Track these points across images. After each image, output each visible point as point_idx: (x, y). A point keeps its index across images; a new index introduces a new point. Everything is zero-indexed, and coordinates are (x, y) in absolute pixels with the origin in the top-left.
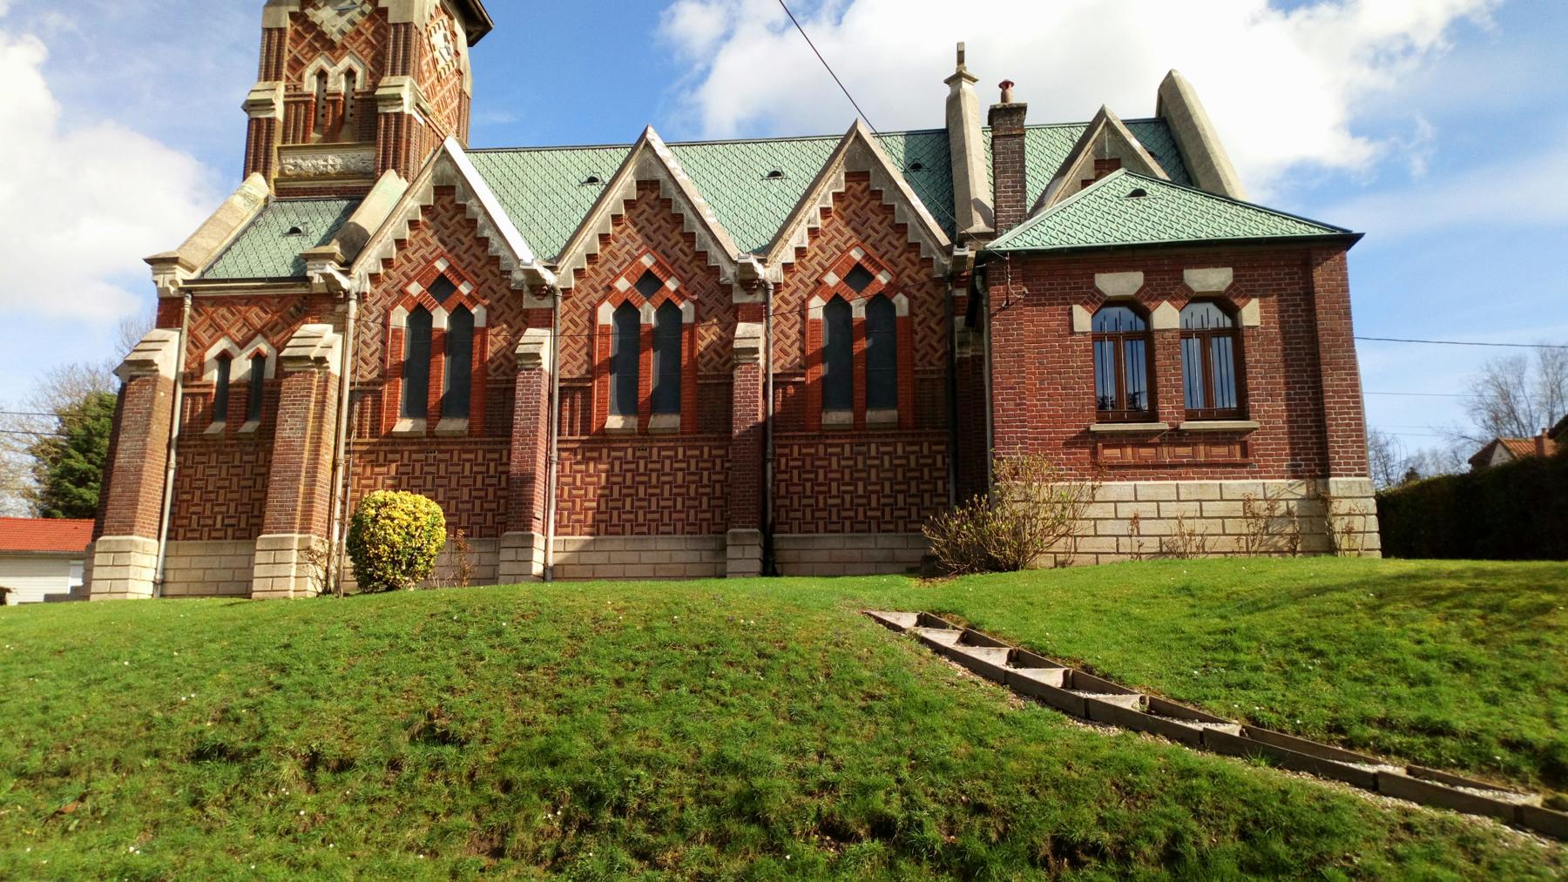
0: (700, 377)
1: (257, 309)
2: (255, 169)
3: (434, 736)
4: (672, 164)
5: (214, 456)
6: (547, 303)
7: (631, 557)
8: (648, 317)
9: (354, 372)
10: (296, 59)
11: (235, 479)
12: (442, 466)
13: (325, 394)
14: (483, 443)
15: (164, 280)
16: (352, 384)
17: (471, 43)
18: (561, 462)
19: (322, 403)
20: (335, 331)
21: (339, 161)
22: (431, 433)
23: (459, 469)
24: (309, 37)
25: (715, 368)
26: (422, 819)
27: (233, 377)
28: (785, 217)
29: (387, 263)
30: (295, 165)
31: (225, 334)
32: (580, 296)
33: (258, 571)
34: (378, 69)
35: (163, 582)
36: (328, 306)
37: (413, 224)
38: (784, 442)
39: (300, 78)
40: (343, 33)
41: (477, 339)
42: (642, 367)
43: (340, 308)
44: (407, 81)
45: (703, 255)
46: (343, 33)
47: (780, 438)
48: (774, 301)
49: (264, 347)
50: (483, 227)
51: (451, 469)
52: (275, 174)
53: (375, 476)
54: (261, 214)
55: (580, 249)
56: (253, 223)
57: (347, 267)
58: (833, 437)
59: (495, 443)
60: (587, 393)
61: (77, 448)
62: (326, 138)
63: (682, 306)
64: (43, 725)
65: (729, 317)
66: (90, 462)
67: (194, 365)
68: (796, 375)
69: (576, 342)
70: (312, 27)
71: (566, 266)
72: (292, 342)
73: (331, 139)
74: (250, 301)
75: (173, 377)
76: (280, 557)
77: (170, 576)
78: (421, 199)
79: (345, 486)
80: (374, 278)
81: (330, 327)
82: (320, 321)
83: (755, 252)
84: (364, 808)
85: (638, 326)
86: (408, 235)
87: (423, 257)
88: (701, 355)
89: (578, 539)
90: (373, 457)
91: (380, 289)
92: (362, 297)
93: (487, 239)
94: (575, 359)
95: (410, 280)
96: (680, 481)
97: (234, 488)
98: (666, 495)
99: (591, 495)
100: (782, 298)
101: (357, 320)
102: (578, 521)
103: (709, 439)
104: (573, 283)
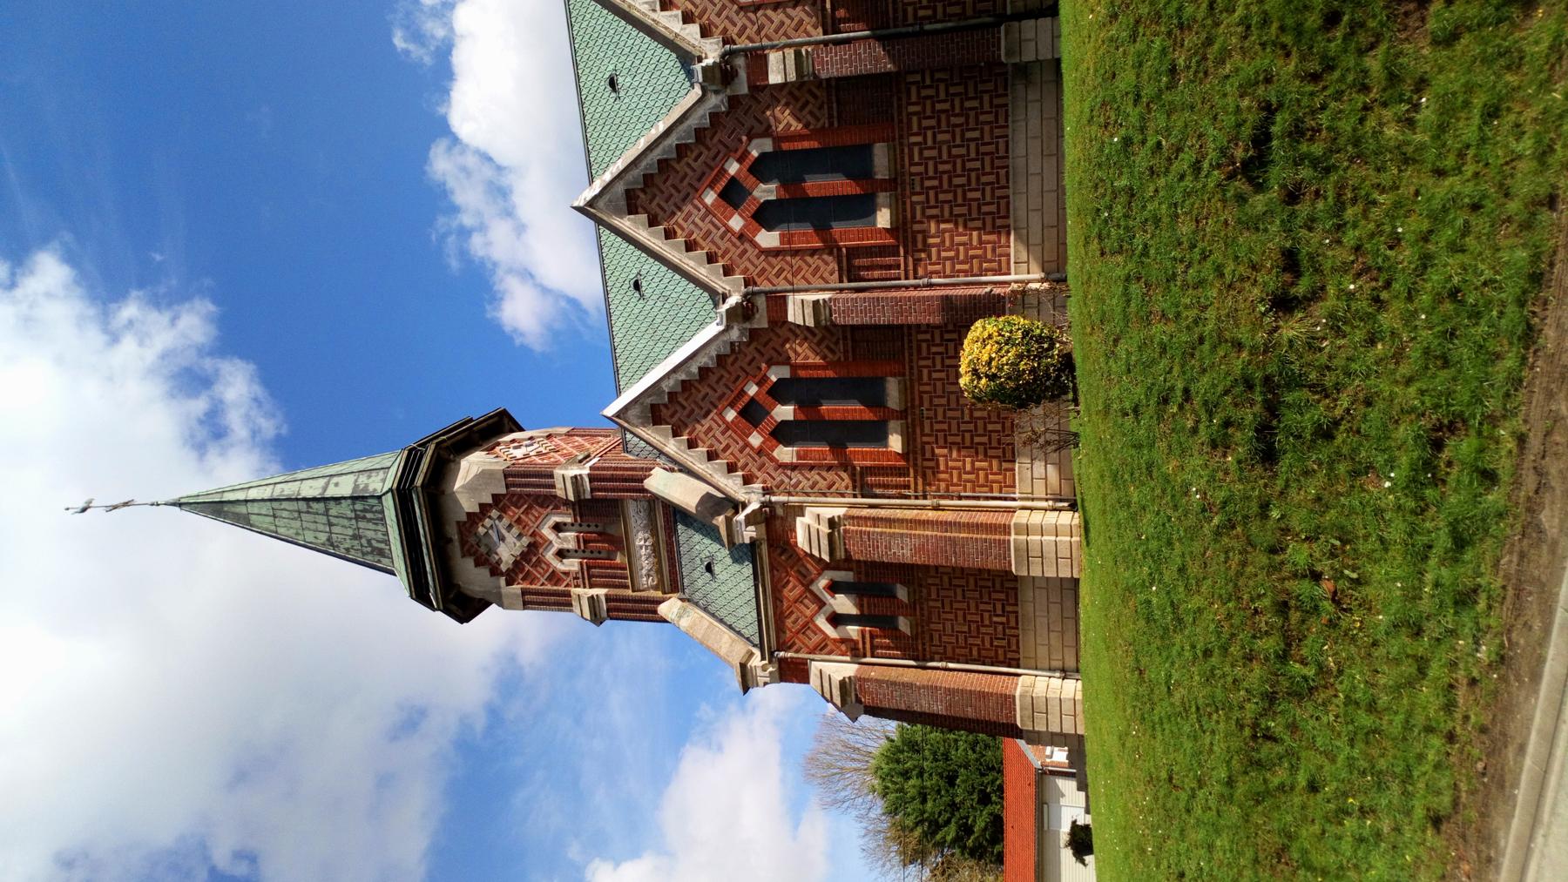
0: (831, 124)
1: (785, 591)
2: (655, 612)
3: (1253, 169)
4: (608, 177)
5: (933, 626)
6: (761, 302)
7: (1035, 184)
8: (769, 191)
9: (843, 495)
10: (549, 579)
11: (956, 605)
12: (936, 401)
13: (866, 519)
14: (911, 361)
15: (762, 677)
16: (855, 496)
17: (521, 429)
18: (930, 274)
19: (876, 521)
20: (803, 515)
21: (641, 535)
22: (902, 415)
23: (939, 384)
24: (527, 567)
25: (821, 108)
26: (1371, 123)
27: (854, 611)
28: (677, 277)
29: (731, 468)
30: (648, 576)
31: (811, 620)
32: (751, 268)
33: (1051, 573)
34: (550, 501)
35: (1063, 670)
36: (778, 522)
37: (692, 444)
38: (900, 14)
39: (567, 574)
40: (520, 536)
41: (802, 373)
42: (823, 193)
43: (780, 512)
44: (558, 472)
45: (699, 133)
46: (520, 536)
47: (895, 19)
48: (743, 43)
49: (823, 582)
50: (689, 373)
51: (939, 392)
52: (659, 594)
53: (948, 470)
54: (697, 604)
55: (703, 270)
56: (705, 610)
57: (737, 506)
58: (904, 210)
59: (911, 348)
60: (854, 252)
61: (934, 833)
62: (620, 549)
63: (755, 154)
64: (1225, 649)
65: (764, 97)
66: (948, 822)
67: (843, 648)
68: (824, 8)
69: (800, 269)
70: (517, 565)
71: (721, 284)
72: (816, 553)
73: (621, 543)
74: (777, 598)
75: (856, 666)
76: (1035, 551)
77: (1058, 664)
78: (666, 437)
79: (960, 498)
80: (747, 480)
81: (799, 520)
82: (793, 530)
83: (716, 305)
84: (1350, 213)
85: (778, 203)
86: (702, 449)
87: (723, 433)
88: (806, 126)
89: (1014, 248)
90: (929, 472)
91: (758, 474)
92: (767, 491)
93: (700, 369)
94: (817, 269)
95: (747, 445)
96: (947, 137)
97: (965, 605)
98: (963, 151)
99: (965, 239)
100: (740, 35)
101: (790, 494)
102: (994, 250)
103: (900, 106)
104: (739, 277)
